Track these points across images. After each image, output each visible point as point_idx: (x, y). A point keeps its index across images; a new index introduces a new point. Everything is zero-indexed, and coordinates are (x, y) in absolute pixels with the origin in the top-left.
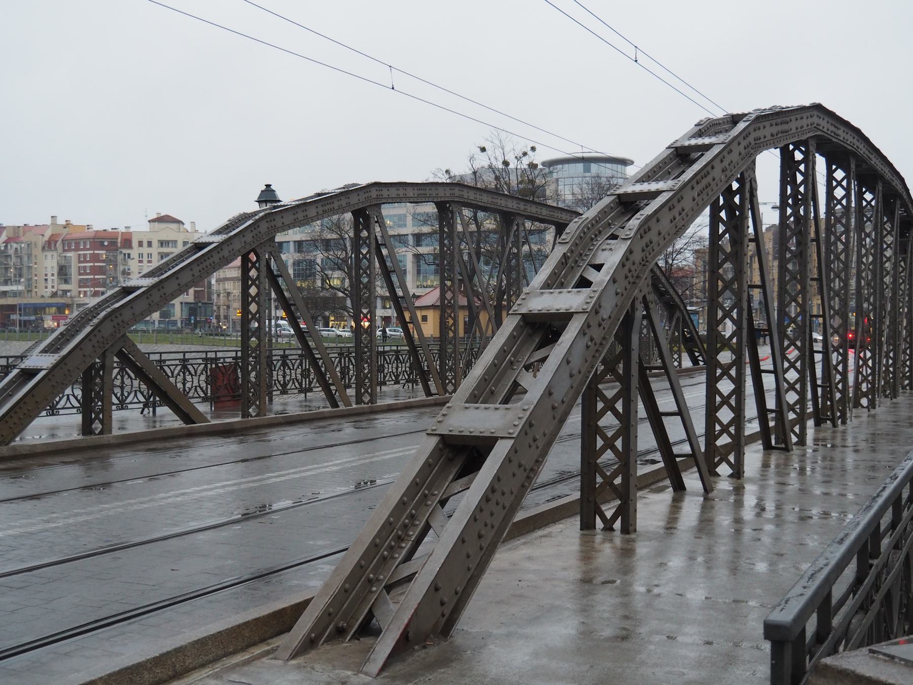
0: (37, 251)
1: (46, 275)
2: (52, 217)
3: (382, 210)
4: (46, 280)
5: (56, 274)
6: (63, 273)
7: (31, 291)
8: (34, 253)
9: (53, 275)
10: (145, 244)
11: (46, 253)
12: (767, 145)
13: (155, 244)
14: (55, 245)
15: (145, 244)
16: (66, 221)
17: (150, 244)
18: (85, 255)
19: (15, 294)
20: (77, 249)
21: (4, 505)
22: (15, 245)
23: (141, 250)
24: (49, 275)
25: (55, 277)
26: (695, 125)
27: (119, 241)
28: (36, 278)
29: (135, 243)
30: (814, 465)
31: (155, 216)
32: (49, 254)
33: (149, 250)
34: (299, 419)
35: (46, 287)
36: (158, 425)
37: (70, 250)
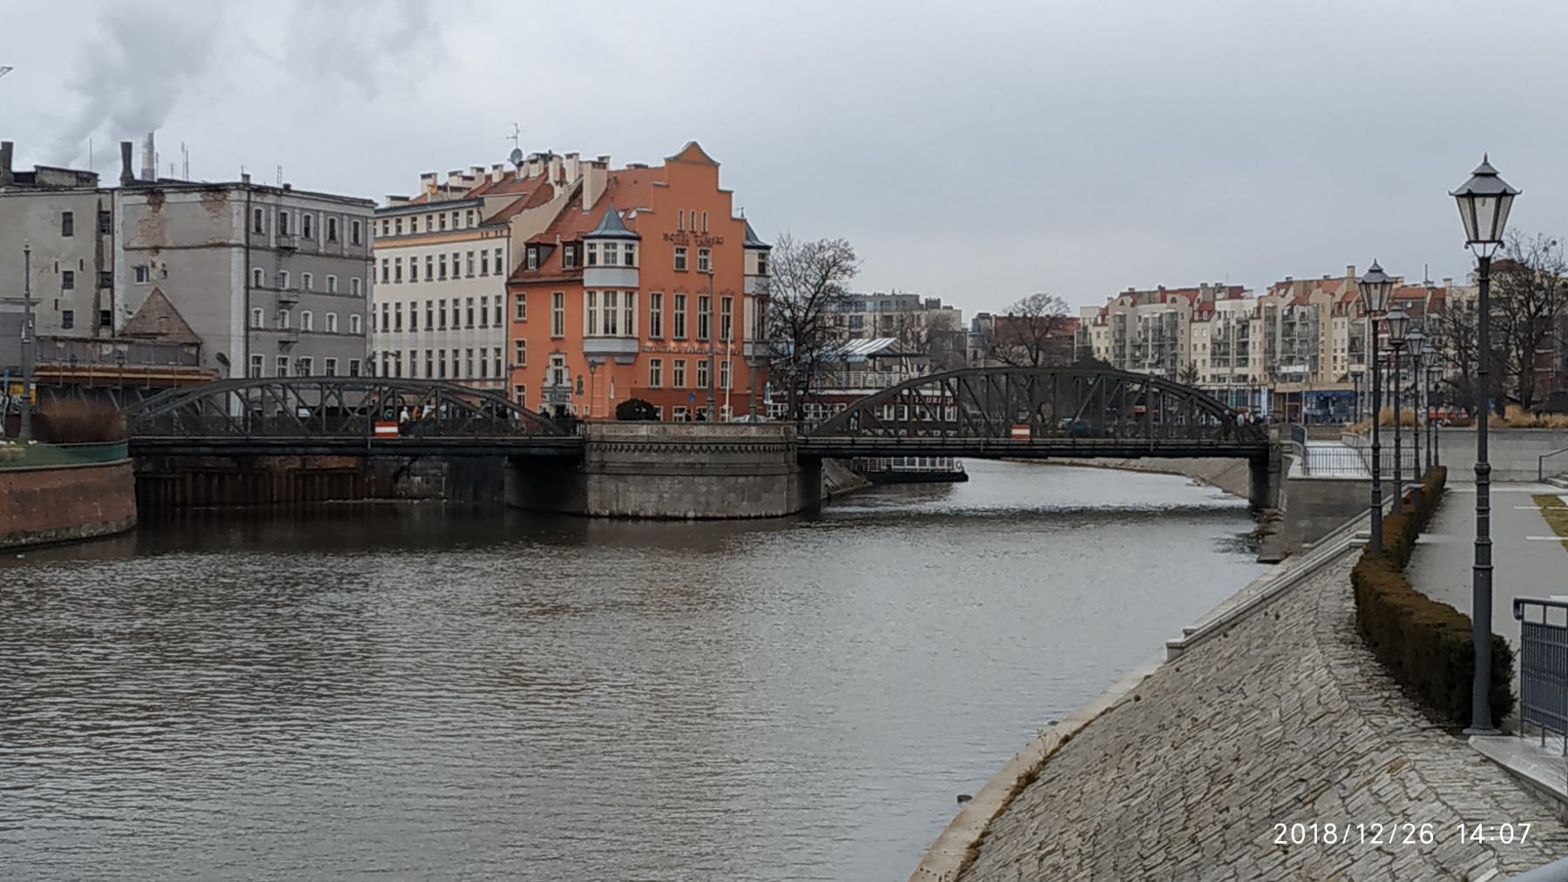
0: (1325, 317)
3: (585, 277)
4: (1335, 358)
5: (1346, 351)
7: (1316, 373)
8: (1321, 319)
11: (1335, 320)
14: (1347, 307)
19: (1298, 378)
21: (3, 475)
22: (1301, 309)
25: (1345, 354)
26: (1476, 175)
28: (1322, 355)
30: (26, 396)
32: (1339, 320)
34: (146, 150)
35: (1335, 368)
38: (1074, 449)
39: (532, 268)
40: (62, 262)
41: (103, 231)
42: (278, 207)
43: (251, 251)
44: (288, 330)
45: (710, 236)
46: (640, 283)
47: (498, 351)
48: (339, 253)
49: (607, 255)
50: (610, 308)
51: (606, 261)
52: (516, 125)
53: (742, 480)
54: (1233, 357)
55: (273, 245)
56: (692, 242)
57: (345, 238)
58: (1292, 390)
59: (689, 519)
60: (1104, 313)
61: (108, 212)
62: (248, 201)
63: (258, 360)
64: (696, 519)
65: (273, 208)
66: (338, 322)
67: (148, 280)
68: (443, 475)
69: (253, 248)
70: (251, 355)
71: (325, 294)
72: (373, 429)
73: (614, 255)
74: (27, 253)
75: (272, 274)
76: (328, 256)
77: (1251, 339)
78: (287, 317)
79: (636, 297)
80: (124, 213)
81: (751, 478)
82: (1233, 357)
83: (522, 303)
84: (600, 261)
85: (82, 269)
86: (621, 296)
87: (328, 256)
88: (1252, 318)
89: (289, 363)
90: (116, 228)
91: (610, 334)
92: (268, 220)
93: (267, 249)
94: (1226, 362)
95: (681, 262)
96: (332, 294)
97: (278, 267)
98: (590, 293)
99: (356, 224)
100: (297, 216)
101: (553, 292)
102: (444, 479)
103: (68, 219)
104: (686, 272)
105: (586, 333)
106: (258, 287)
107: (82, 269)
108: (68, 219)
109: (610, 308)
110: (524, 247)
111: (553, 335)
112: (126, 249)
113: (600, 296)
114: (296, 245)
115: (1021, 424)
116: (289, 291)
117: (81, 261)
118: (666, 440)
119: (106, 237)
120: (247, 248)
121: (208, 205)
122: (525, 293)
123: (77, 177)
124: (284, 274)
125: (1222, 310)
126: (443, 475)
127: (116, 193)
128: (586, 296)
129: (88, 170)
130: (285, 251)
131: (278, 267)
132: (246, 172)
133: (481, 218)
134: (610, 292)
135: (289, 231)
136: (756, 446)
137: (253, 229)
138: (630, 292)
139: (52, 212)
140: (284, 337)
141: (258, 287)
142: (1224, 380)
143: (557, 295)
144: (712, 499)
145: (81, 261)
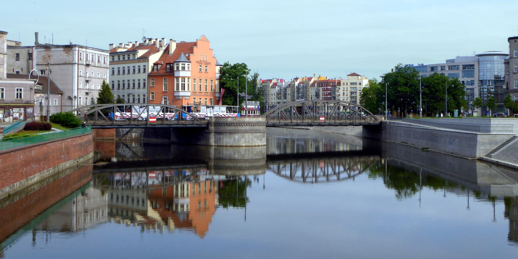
1: (312, 96)
2: (110, 45)
5: (315, 96)
6: (317, 95)
9: (314, 96)
10: (345, 84)
12: (239, 167)
13: (349, 84)
15: (345, 84)
16: (70, 43)
17: (347, 84)
18: (324, 88)
20: (322, 86)
23: (344, 86)
24: (313, 96)
27: (336, 83)
29: (342, 84)
31: (350, 73)
33: (347, 86)
36: (502, 68)
37: (320, 87)
38: (330, 124)
39: (155, 71)
40: (16, 68)
41: (29, 59)
42: (86, 52)
43: (79, 65)
44: (88, 89)
45: (208, 62)
47: (144, 95)
48: (100, 66)
50: (183, 83)
52: (144, 29)
53: (258, 134)
55: (85, 64)
56: (203, 64)
57: (102, 62)
59: (243, 146)
60: (290, 85)
61: (31, 54)
62: (79, 50)
63: (80, 98)
64: (245, 146)
65: (85, 52)
67: (44, 74)
68: (142, 133)
69: (81, 64)
70: (79, 97)
71: (97, 78)
72: (319, 119)
73: (184, 67)
75: (84, 72)
76: (98, 67)
77: (288, 93)
79: (190, 79)
80: (37, 54)
81: (260, 133)
85: (22, 71)
86: (186, 79)
87: (98, 67)
88: (288, 87)
89: (88, 99)
90: (34, 58)
91: (183, 90)
92: (83, 56)
93: (83, 65)
94: (280, 99)
95: (200, 69)
96: (99, 78)
97: (86, 70)
98: (177, 78)
99: (99, 56)
100: (91, 55)
101: (164, 78)
102: (143, 134)
103: (18, 55)
104: (207, 73)
105: (175, 90)
106: (81, 76)
107: (22, 71)
108: (18, 55)
110: (153, 65)
112: (37, 65)
114: (90, 63)
115: (322, 117)
116: (89, 77)
117: (22, 68)
118: (236, 122)
119: (30, 61)
120: (78, 64)
121: (65, 51)
123: (16, 43)
124: (87, 72)
125: (279, 85)
127: (34, 48)
129: (19, 41)
130: (88, 65)
131: (86, 70)
132: (71, 42)
134: (184, 78)
135: (88, 60)
136: (258, 124)
137: (79, 59)
139: (12, 53)
140: (87, 91)
141: (81, 76)
142: (280, 103)
143: (165, 79)
144: (250, 140)
145: (22, 68)
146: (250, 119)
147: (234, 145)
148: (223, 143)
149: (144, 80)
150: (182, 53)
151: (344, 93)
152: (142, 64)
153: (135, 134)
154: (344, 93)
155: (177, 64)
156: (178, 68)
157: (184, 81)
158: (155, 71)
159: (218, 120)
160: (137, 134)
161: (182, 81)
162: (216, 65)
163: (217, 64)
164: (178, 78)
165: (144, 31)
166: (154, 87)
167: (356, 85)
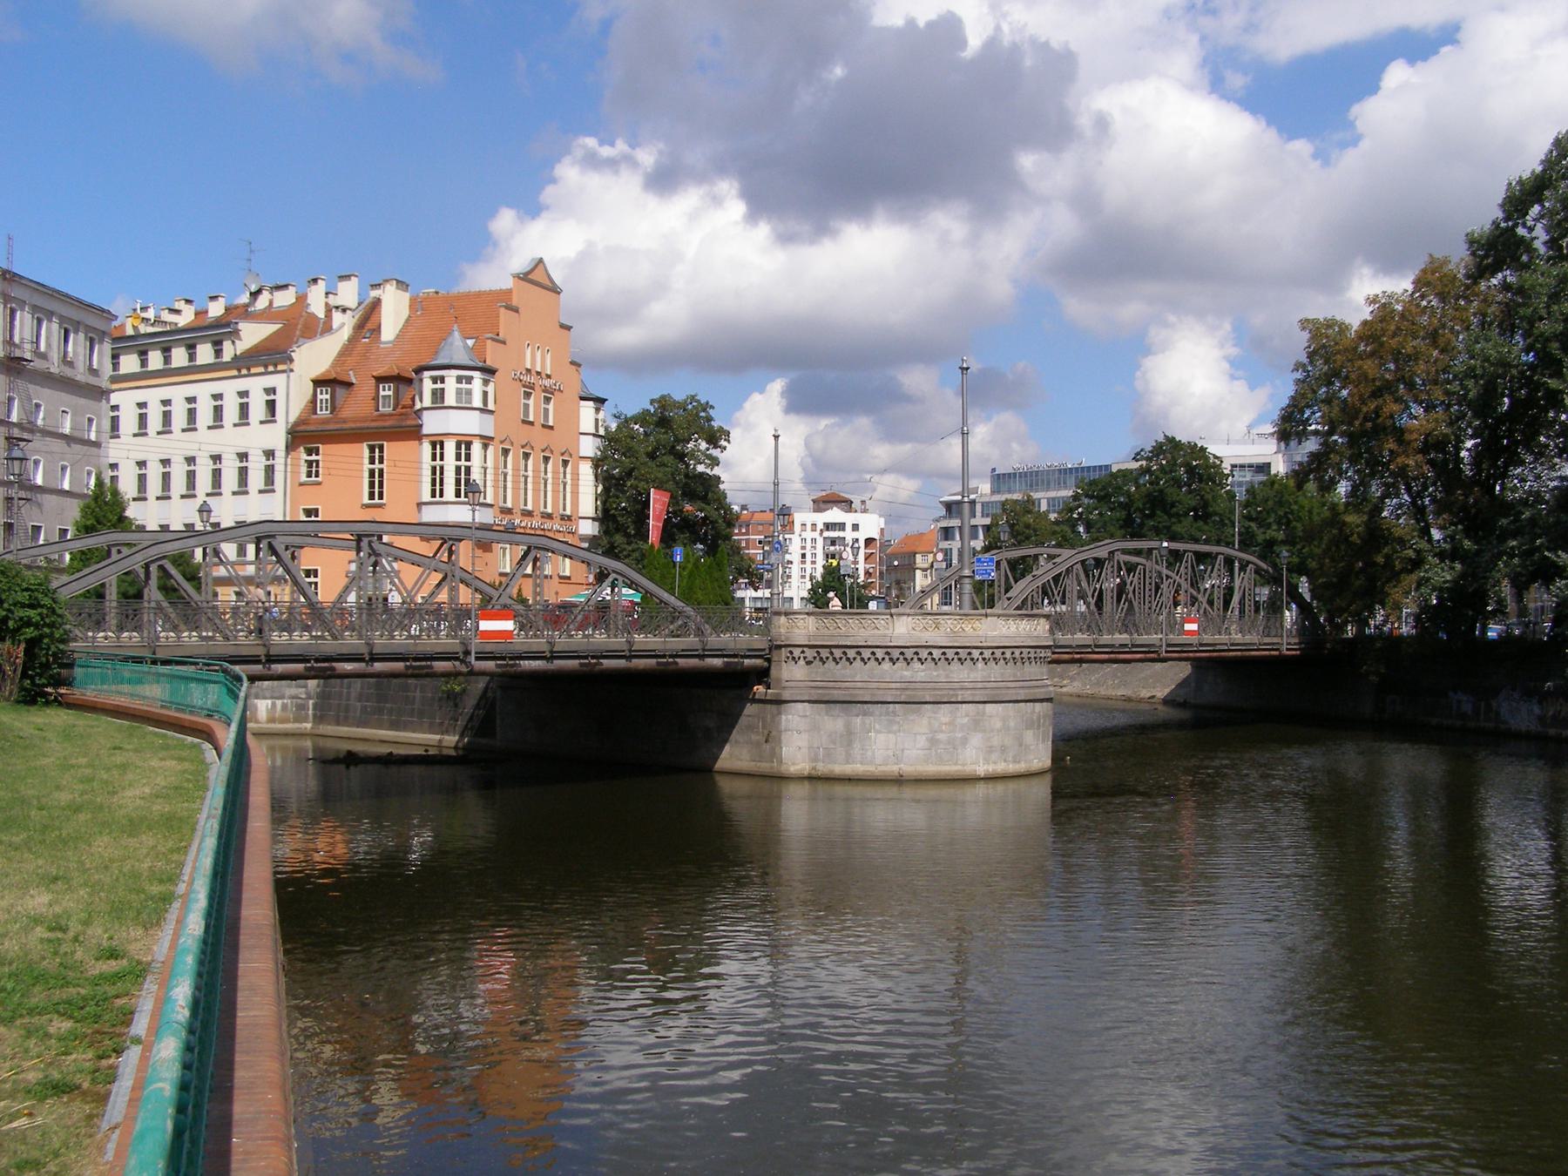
10: (809, 527)
33: (973, 522)
39: (323, 413)
46: (578, 440)
49: (459, 392)
50: (463, 463)
51: (458, 399)
54: (377, 461)
58: (276, 468)
66: (71, 475)
68: (309, 697)
73: (469, 392)
74: (776, 437)
78: (508, 551)
82: (377, 461)
83: (314, 457)
84: (450, 399)
86: (476, 447)
91: (463, 499)
102: (311, 702)
105: (426, 497)
109: (463, 463)
111: (366, 500)
113: (450, 447)
122: (385, 443)
126: (309, 697)
128: (427, 448)
133: (235, 349)
134: (464, 445)
138: (486, 441)
143: (372, 449)
146: (1013, 628)
147: (839, 769)
148: (192, 701)
149: (270, 454)
150: (455, 327)
151: (804, 556)
152: (256, 385)
153: (269, 702)
154: (804, 556)
155: (435, 380)
156: (438, 396)
157: (468, 458)
158: (323, 413)
159: (832, 631)
160: (279, 703)
161: (458, 458)
162: (582, 399)
163: (584, 395)
164: (437, 444)
165: (251, 251)
166: (319, 484)
167: (844, 530)
